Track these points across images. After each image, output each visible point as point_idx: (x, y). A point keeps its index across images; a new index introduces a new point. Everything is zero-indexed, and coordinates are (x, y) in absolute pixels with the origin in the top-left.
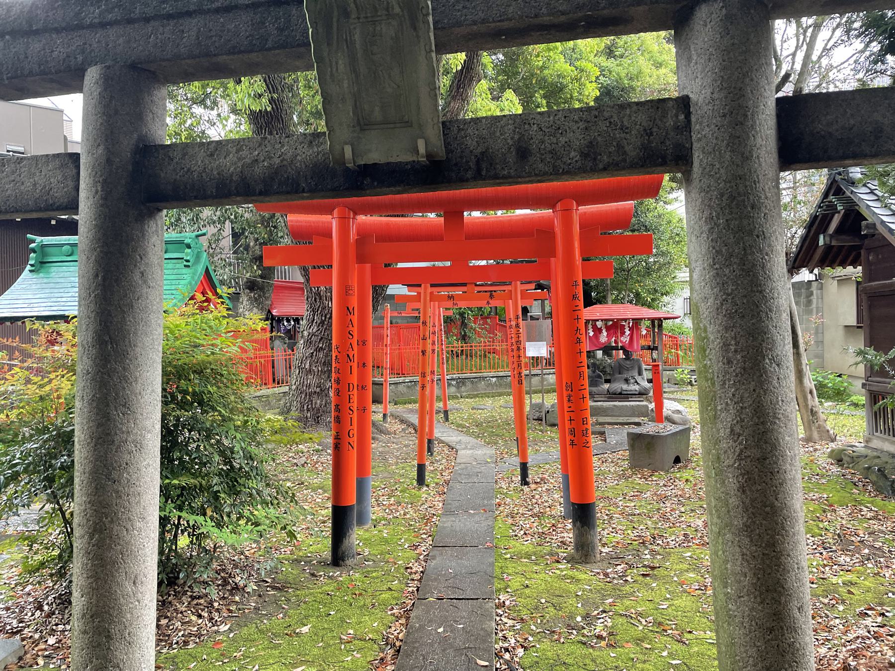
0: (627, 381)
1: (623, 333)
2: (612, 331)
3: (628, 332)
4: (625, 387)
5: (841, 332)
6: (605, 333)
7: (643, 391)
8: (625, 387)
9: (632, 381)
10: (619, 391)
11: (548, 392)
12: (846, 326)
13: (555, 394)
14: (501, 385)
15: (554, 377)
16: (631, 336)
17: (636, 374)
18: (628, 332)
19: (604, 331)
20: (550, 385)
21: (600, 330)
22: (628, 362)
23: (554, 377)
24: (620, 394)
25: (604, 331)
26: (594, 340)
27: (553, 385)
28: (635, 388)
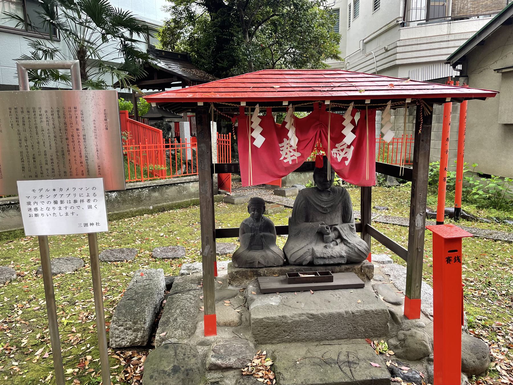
1: (339, 138)
2: (311, 134)
3: (349, 137)
4: (319, 249)
6: (293, 139)
7: (355, 257)
8: (319, 249)
9: (332, 235)
10: (309, 258)
11: (186, 206)
12: (506, 125)
13: (198, 208)
14: (124, 201)
15: (197, 185)
16: (358, 144)
17: (337, 220)
18: (349, 137)
19: (291, 134)
20: (190, 195)
21: (282, 134)
22: (325, 197)
23: (197, 185)
25: (291, 134)
26: (265, 158)
27: (194, 194)
28: (339, 250)
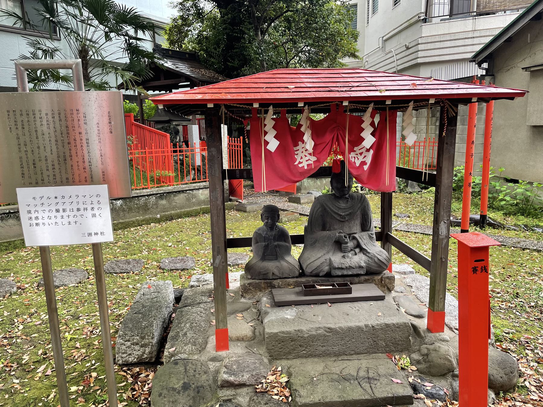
0: (339, 245)
1: (358, 141)
2: (328, 137)
3: (369, 140)
4: (337, 259)
5: (524, 134)
6: (309, 143)
7: (375, 268)
8: (337, 259)
9: (351, 244)
10: (326, 269)
12: (535, 127)
13: (208, 216)
14: (130, 209)
15: (207, 192)
17: (356, 228)
18: (369, 140)
19: (307, 137)
20: (200, 203)
22: (342, 204)
23: (207, 192)
24: (328, 275)
25: (307, 137)
26: (279, 163)
27: (204, 202)
28: (357, 260)
